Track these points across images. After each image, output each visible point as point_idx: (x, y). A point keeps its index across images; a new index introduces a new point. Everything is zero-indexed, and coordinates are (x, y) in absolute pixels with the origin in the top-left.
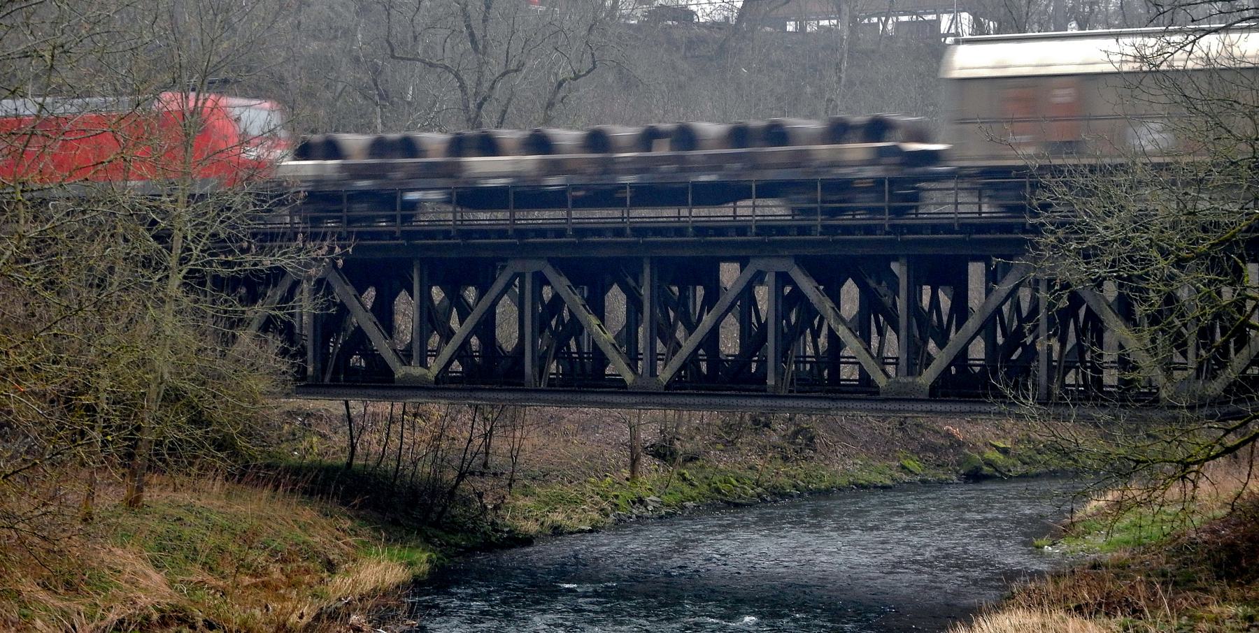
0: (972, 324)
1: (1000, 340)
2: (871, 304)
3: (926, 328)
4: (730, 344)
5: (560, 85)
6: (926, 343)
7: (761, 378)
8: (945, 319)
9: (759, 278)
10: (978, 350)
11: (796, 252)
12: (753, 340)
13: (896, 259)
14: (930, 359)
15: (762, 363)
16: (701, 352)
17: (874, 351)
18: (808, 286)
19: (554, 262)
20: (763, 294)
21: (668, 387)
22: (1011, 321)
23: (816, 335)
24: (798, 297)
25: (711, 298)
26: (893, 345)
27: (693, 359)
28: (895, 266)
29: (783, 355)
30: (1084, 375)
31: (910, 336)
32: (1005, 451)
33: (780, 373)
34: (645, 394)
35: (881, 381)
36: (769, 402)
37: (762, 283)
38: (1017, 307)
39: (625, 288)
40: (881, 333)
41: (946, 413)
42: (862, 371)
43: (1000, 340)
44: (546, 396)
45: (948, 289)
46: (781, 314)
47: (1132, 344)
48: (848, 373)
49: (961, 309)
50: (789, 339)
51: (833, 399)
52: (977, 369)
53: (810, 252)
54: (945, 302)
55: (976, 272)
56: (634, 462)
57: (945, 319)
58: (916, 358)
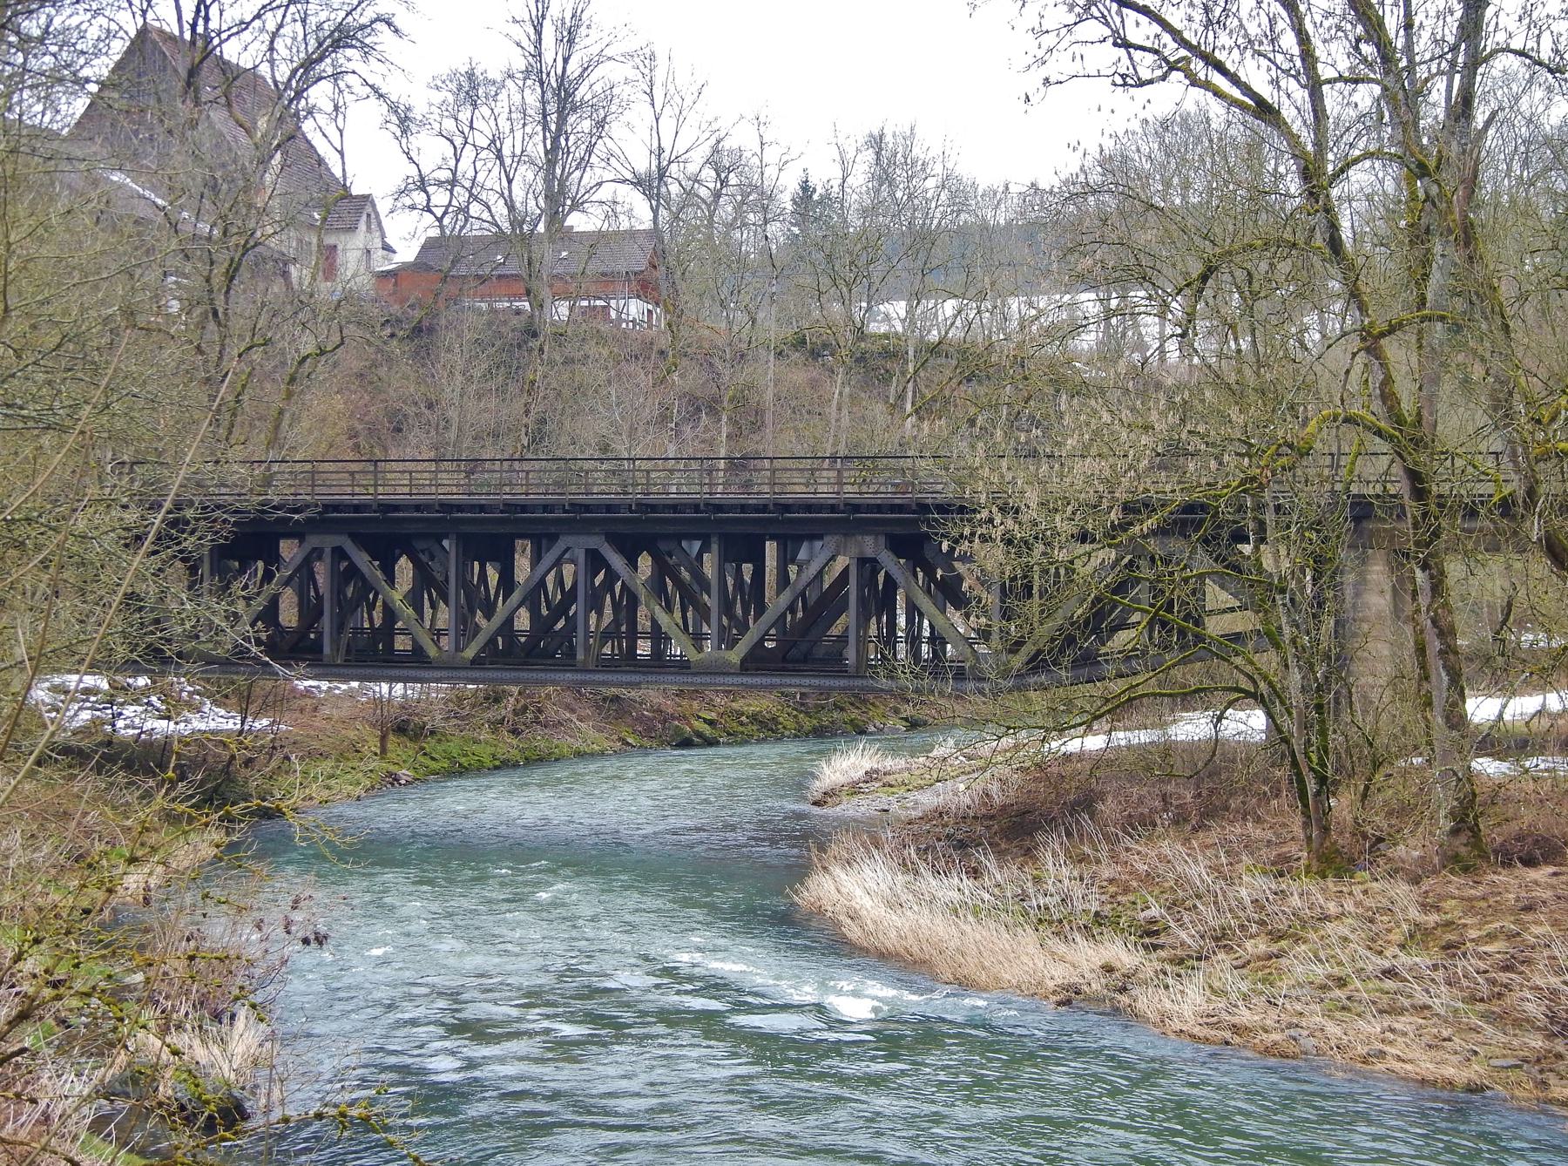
0: (516, 596)
1: (545, 612)
2: (425, 580)
3: (476, 601)
4: (289, 616)
5: (304, 359)
6: (474, 614)
7: (317, 648)
8: (492, 592)
9: (317, 553)
10: (523, 621)
11: (889, 529)
12: (310, 612)
13: (447, 537)
14: (477, 629)
15: (320, 635)
16: (773, 631)
17: (427, 624)
18: (362, 559)
19: (354, 537)
20: (321, 571)
21: (473, 662)
22: (555, 595)
23: (372, 607)
24: (353, 572)
25: (507, 582)
26: (445, 616)
27: (492, 641)
28: (446, 543)
29: (340, 627)
30: (620, 645)
31: (458, 606)
32: (711, 723)
33: (335, 642)
34: (448, 668)
35: (432, 652)
36: (579, 677)
37: (320, 558)
38: (560, 581)
39: (413, 559)
40: (433, 606)
41: (766, 687)
42: (414, 641)
43: (545, 612)
44: (345, 671)
45: (498, 565)
46: (338, 591)
47: (663, 619)
48: (401, 643)
49: (507, 582)
50: (346, 608)
51: (644, 673)
52: (523, 639)
53: (622, 529)
54: (493, 576)
55: (771, 548)
56: (383, 739)
57: (492, 592)
58: (465, 629)
